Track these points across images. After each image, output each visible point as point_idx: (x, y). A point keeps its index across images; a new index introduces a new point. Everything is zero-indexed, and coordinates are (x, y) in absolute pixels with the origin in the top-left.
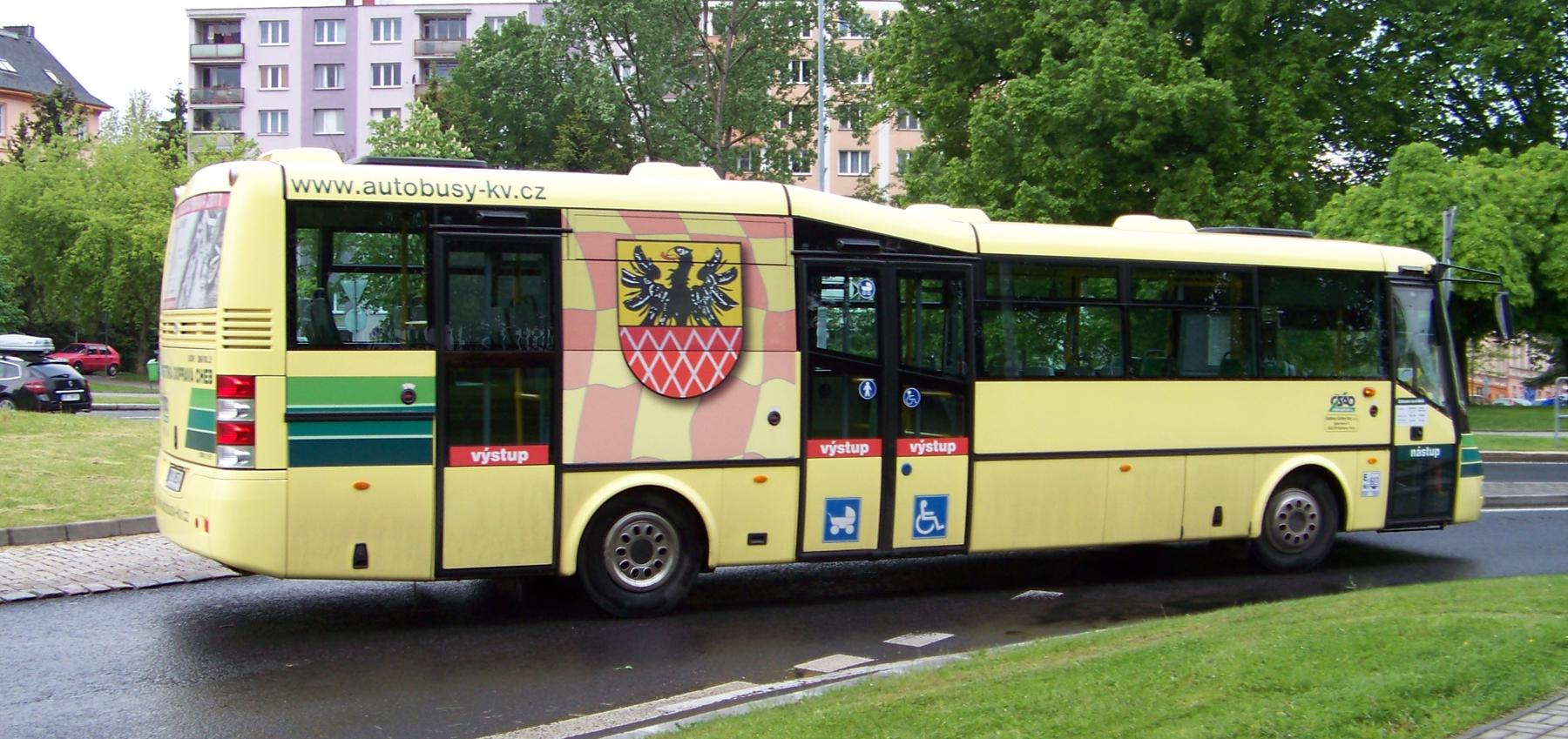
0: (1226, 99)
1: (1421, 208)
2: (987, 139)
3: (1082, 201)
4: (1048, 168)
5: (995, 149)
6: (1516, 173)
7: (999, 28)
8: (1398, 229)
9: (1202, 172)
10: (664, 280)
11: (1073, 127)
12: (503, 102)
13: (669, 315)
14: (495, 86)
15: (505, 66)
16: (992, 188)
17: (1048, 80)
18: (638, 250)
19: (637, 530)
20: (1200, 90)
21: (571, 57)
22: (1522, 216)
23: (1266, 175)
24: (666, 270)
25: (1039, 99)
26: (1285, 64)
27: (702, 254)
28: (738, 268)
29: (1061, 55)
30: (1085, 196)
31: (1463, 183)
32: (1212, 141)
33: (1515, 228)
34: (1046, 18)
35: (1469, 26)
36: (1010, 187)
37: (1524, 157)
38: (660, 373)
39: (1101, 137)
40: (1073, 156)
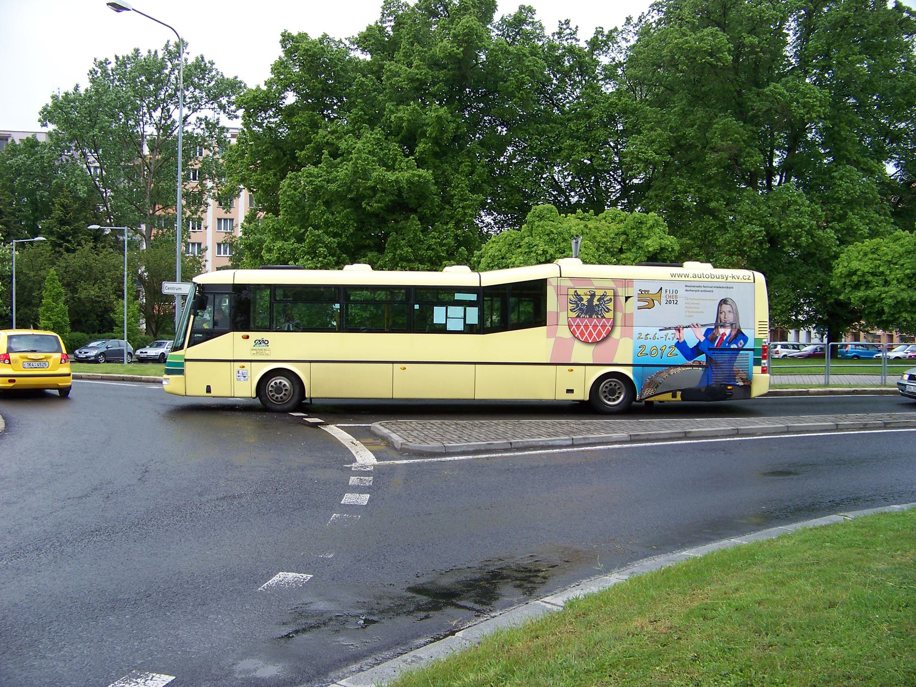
0: (429, 181)
1: (546, 243)
2: (290, 202)
3: (344, 239)
4: (325, 220)
5: (294, 209)
6: (598, 224)
7: (298, 139)
8: (533, 254)
9: (414, 223)
10: (585, 302)
11: (339, 196)
12: (23, 185)
13: (586, 314)
14: (19, 175)
15: (24, 163)
16: (292, 231)
17: (325, 169)
18: (576, 291)
19: (611, 385)
20: (414, 175)
21: (64, 160)
22: (603, 249)
23: (450, 225)
24: (586, 299)
25: (320, 179)
26: (462, 163)
27: (599, 293)
28: (612, 297)
29: (334, 155)
30: (346, 236)
31: (570, 227)
32: (420, 206)
33: (600, 256)
34: (325, 133)
35: (565, 144)
36: (303, 230)
37: (601, 215)
38: (582, 334)
39: (355, 203)
40: (339, 213)
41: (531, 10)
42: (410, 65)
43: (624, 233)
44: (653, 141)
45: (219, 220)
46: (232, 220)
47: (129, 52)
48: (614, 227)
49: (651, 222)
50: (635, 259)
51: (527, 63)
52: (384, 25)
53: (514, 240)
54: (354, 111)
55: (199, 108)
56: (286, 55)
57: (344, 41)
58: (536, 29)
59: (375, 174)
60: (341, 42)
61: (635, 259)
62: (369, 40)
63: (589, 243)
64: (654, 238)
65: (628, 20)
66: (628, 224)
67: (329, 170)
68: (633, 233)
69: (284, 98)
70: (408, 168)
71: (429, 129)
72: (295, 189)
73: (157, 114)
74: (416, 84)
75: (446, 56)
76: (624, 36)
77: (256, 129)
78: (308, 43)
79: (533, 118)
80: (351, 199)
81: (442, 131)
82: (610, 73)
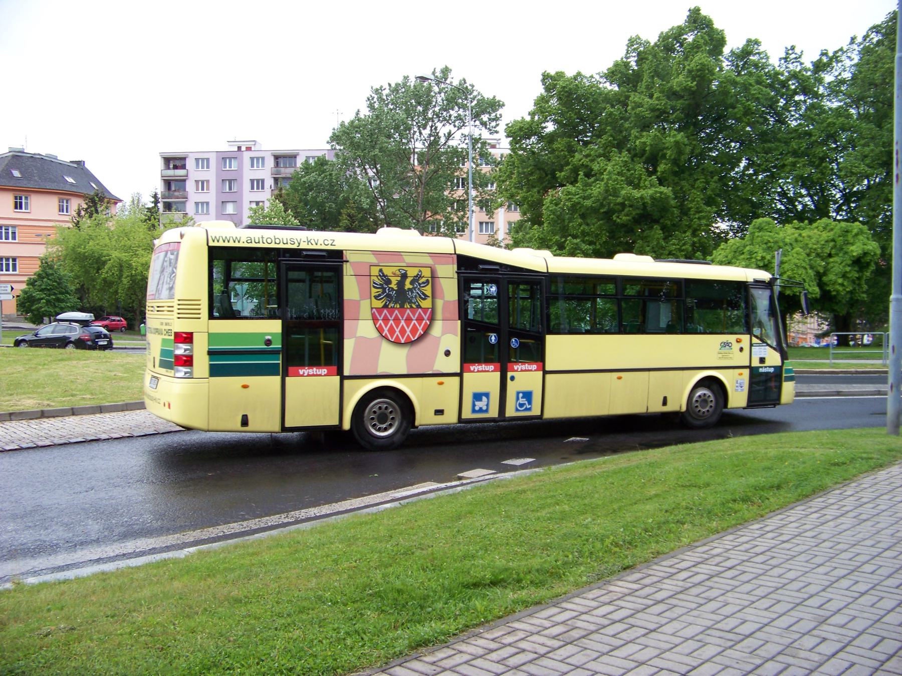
0: (669, 196)
1: (764, 250)
2: (552, 216)
3: (598, 247)
5: (556, 221)
8: (753, 260)
11: (594, 210)
12: (315, 198)
14: (311, 190)
15: (315, 180)
20: (656, 192)
23: (688, 234)
25: (577, 196)
26: (698, 179)
29: (588, 175)
30: (600, 244)
32: (662, 217)
34: (581, 157)
36: (563, 240)
37: (815, 225)
38: (392, 331)
39: (608, 215)
41: (757, 43)
42: (651, 96)
43: (833, 240)
44: (866, 156)
45: (481, 223)
46: (492, 223)
47: (400, 80)
48: (825, 235)
49: (855, 231)
50: (842, 263)
51: (753, 92)
52: (629, 60)
53: (738, 248)
54: (604, 137)
55: (463, 125)
56: (546, 91)
57: (595, 76)
58: (762, 58)
59: (623, 192)
60: (592, 77)
61: (842, 263)
62: (618, 73)
63: (801, 250)
64: (858, 244)
65: (853, 40)
66: (836, 233)
67: (584, 188)
68: (840, 240)
69: (545, 127)
70: (651, 186)
71: (669, 152)
72: (556, 205)
73: (426, 132)
74: (657, 113)
75: (682, 90)
76: (849, 54)
77: (521, 152)
78: (565, 81)
79: (764, 137)
80: (603, 212)
81: (680, 153)
82: (834, 89)
